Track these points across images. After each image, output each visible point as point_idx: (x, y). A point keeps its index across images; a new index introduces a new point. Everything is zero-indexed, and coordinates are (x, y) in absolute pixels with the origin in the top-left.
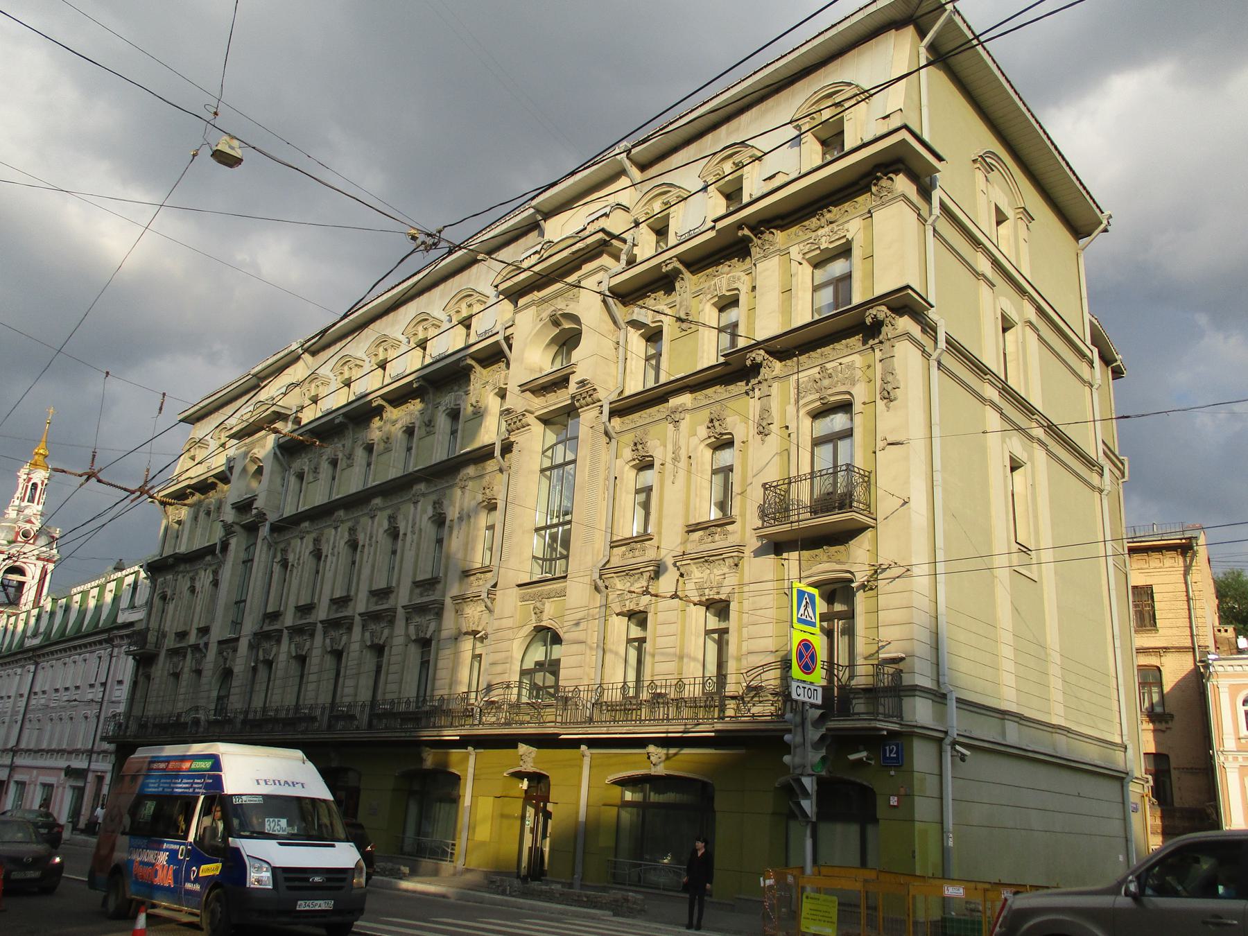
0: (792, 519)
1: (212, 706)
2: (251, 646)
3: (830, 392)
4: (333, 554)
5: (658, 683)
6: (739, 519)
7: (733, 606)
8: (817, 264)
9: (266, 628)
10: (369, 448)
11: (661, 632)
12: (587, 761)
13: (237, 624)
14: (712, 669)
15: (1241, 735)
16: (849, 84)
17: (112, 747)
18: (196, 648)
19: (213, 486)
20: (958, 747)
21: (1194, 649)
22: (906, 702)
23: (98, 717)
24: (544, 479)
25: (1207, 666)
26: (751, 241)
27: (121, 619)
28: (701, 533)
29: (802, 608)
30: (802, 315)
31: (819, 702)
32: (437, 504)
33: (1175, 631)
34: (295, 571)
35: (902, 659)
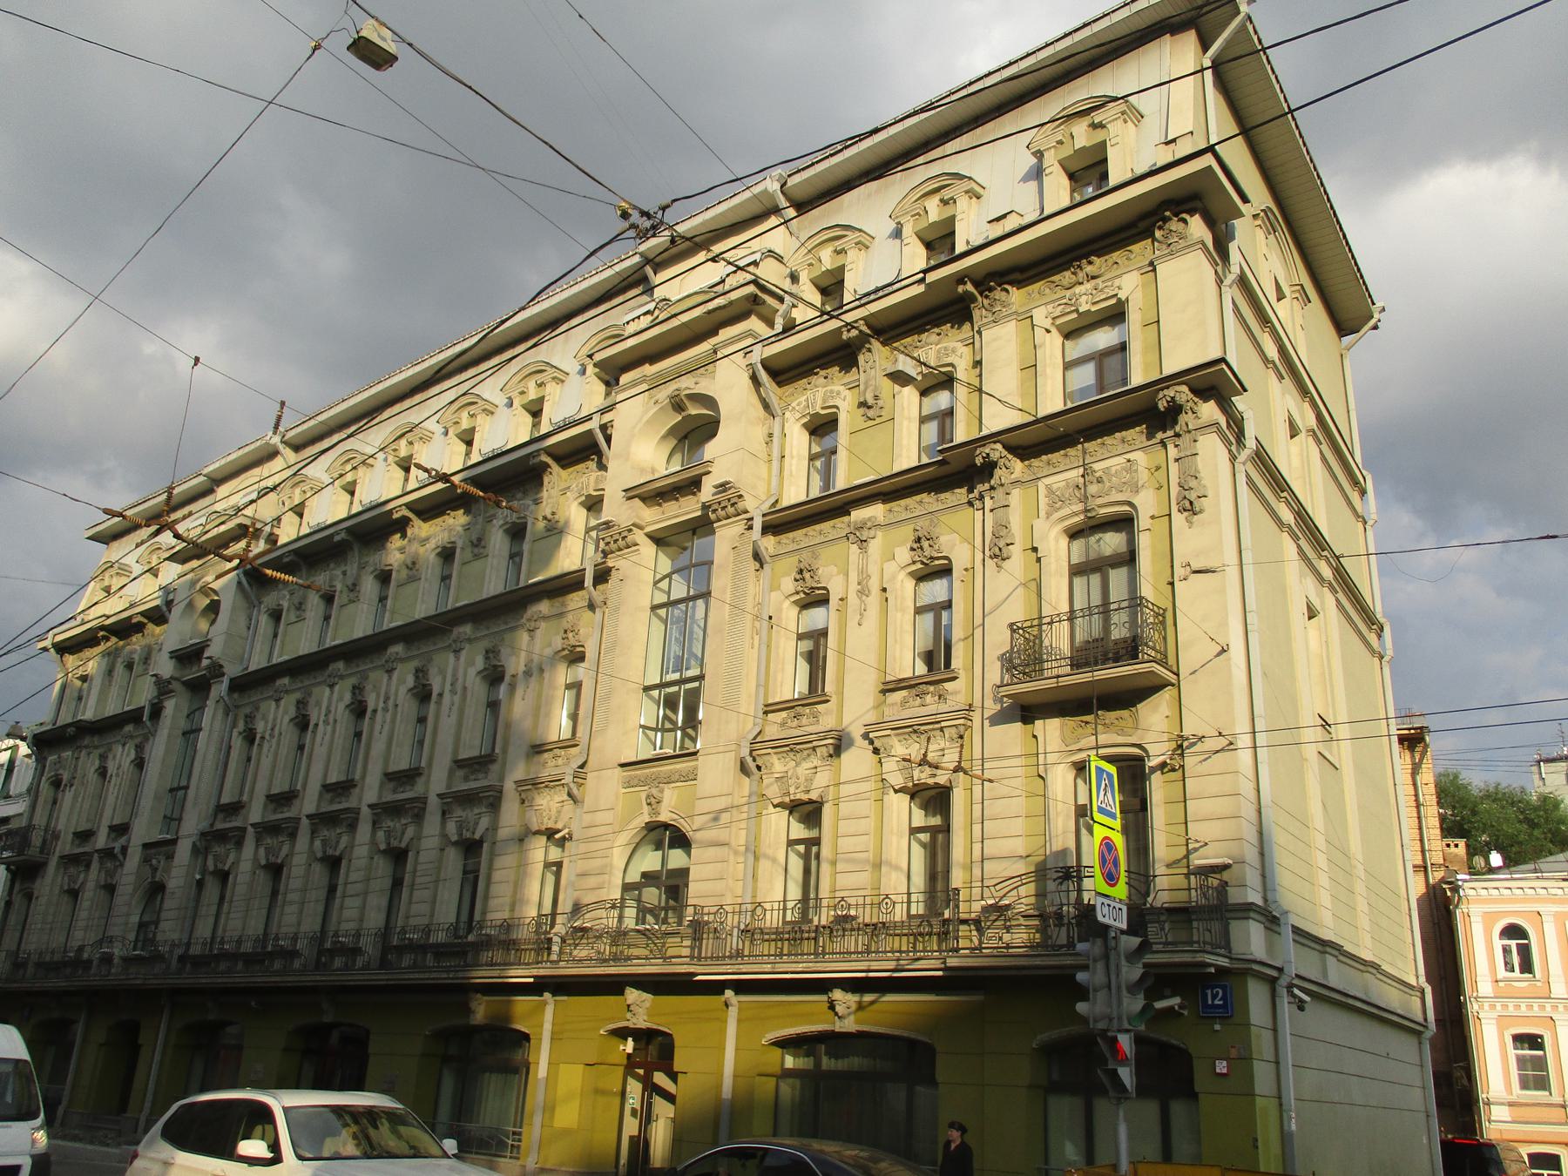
1: (132, 936)
2: (196, 851)
3: (1100, 501)
4: (326, 722)
5: (852, 901)
6: (962, 674)
7: (827, 811)
8: (1070, 334)
9: (219, 826)
10: (384, 577)
11: (845, 830)
12: (733, 1012)
13: (172, 820)
14: (795, 893)
15: (1499, 977)
18: (108, 854)
19: (139, 628)
20: (1296, 991)
21: (1425, 868)
22: (1236, 927)
24: (656, 622)
25: (1456, 889)
26: (974, 300)
28: (904, 693)
30: (1052, 402)
32: (491, 653)
34: (266, 745)
35: (1226, 867)
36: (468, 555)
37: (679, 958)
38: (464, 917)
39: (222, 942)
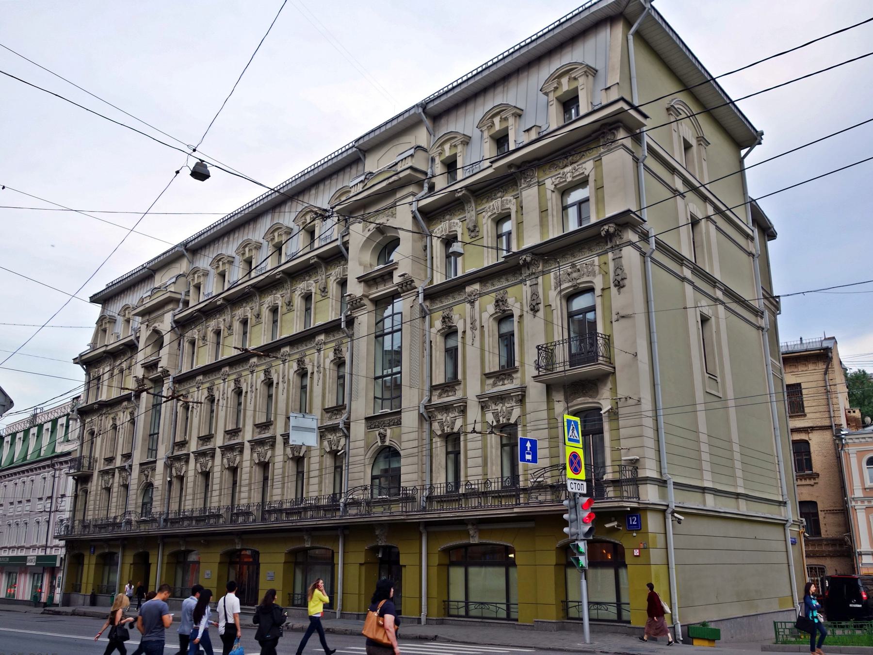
1: (139, 510)
5: (472, 482)
11: (471, 446)
13: (152, 450)
15: (867, 486)
16: (581, 64)
17: (63, 543)
18: (122, 469)
20: (676, 515)
23: (48, 522)
27: (59, 449)
29: (571, 432)
31: (585, 492)
33: (818, 415)
34: (195, 411)
36: (285, 309)
37: (397, 512)
38: (299, 496)
39: (184, 512)
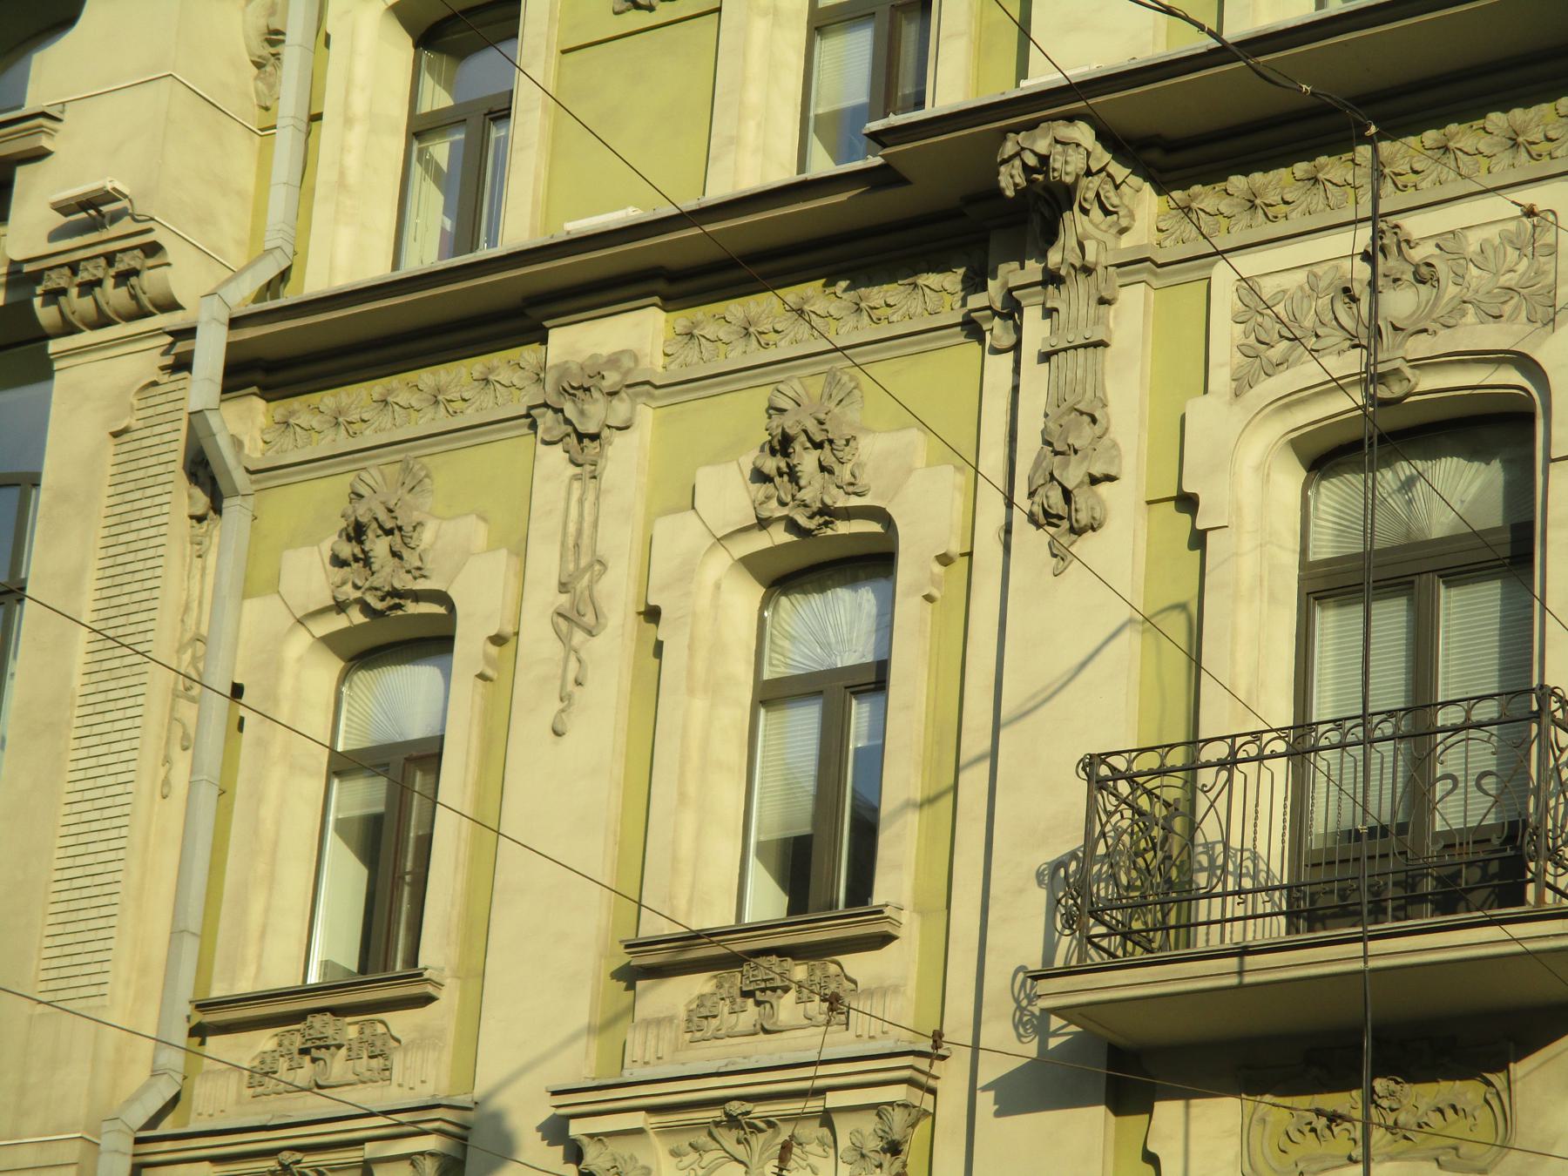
0: (1204, 939)
3: (1419, 347)
6: (910, 928)
28: (701, 983)
